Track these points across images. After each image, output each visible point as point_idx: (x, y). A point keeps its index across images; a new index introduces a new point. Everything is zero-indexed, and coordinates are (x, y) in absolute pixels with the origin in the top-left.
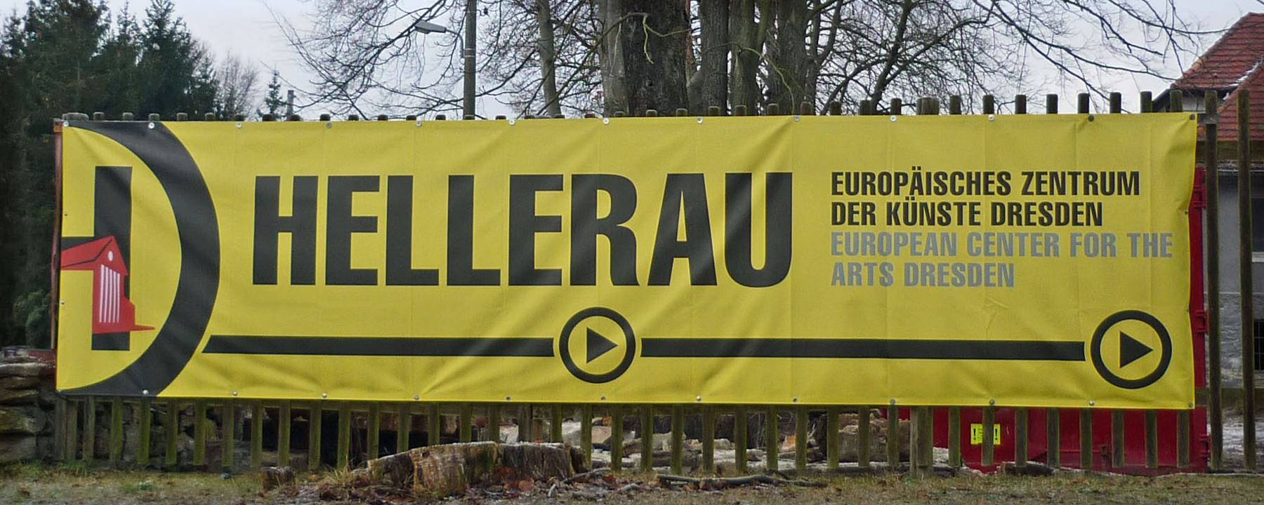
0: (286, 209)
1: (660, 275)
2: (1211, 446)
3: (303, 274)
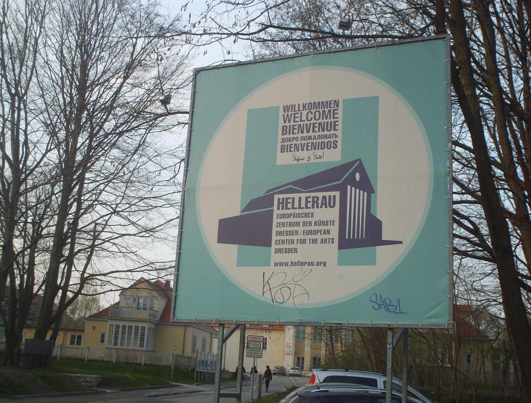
0: (281, 201)
1: (321, 207)
2: (311, 385)
3: (283, 209)
